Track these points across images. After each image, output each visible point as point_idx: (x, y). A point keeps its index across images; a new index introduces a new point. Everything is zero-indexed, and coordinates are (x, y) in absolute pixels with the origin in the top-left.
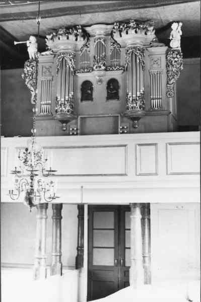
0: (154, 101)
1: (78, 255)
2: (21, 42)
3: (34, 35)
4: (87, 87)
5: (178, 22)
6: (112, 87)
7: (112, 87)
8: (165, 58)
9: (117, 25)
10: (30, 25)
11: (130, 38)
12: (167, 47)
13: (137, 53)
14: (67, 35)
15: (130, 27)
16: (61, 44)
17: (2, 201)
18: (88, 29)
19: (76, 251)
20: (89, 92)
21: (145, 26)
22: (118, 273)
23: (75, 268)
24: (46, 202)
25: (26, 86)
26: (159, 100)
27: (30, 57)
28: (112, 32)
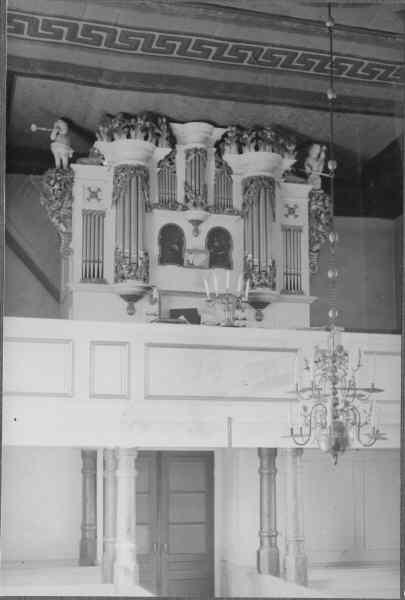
0: (96, 265)
1: (84, 538)
2: (44, 129)
3: (65, 119)
5: (321, 143)
6: (216, 244)
7: (216, 244)
8: (307, 204)
9: (232, 131)
10: (66, 96)
11: (252, 162)
13: (263, 187)
14: (126, 130)
15: (133, 127)
16: (126, 150)
18: (176, 127)
19: (80, 532)
20: (176, 247)
21: (110, 126)
22: (284, 561)
23: (76, 562)
24: (297, 446)
25: (49, 221)
26: (96, 265)
27: (58, 163)
28: (222, 141)
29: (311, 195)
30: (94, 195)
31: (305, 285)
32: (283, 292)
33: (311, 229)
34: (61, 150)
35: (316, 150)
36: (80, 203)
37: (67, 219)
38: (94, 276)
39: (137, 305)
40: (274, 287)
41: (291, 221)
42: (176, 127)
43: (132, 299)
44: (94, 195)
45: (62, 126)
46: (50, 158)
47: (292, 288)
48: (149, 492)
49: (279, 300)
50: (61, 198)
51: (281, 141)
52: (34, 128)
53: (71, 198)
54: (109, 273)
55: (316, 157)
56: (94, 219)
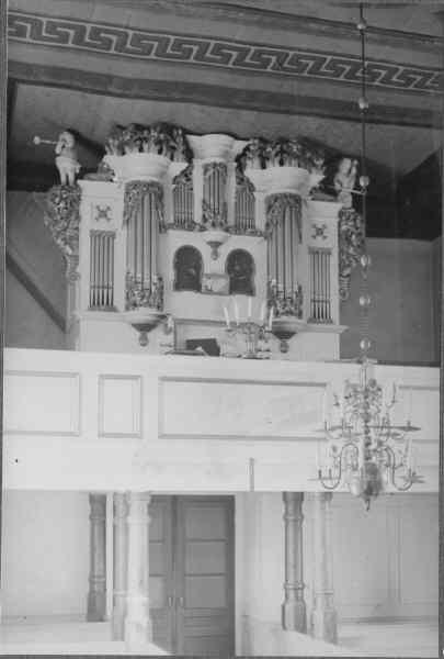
0: (105, 291)
1: (92, 591)
2: (48, 142)
3: (71, 131)
4: (188, 263)
5: (352, 157)
6: (237, 268)
7: (237, 268)
8: (336, 224)
9: (254, 144)
10: (72, 105)
11: (276, 178)
12: (186, 165)
13: (288, 205)
14: (138, 142)
16: (138, 165)
17: (434, 375)
18: (192, 139)
19: (88, 584)
20: (193, 271)
23: (84, 618)
25: (54, 242)
26: (105, 291)
27: (63, 179)
28: (244, 154)
29: (341, 214)
30: (103, 214)
31: (335, 313)
32: (310, 321)
33: (341, 252)
34: (66, 165)
35: (346, 165)
36: (88, 223)
37: (73, 241)
38: (103, 303)
39: (150, 335)
40: (300, 315)
41: (319, 243)
42: (192, 139)
43: (144, 328)
44: (103, 214)
45: (68, 138)
46: (55, 174)
47: (320, 316)
48: (163, 541)
49: (306, 330)
50: (67, 218)
51: (308, 155)
52: (37, 140)
53: (78, 218)
54: (120, 300)
55: (346, 173)
56: (103, 241)
